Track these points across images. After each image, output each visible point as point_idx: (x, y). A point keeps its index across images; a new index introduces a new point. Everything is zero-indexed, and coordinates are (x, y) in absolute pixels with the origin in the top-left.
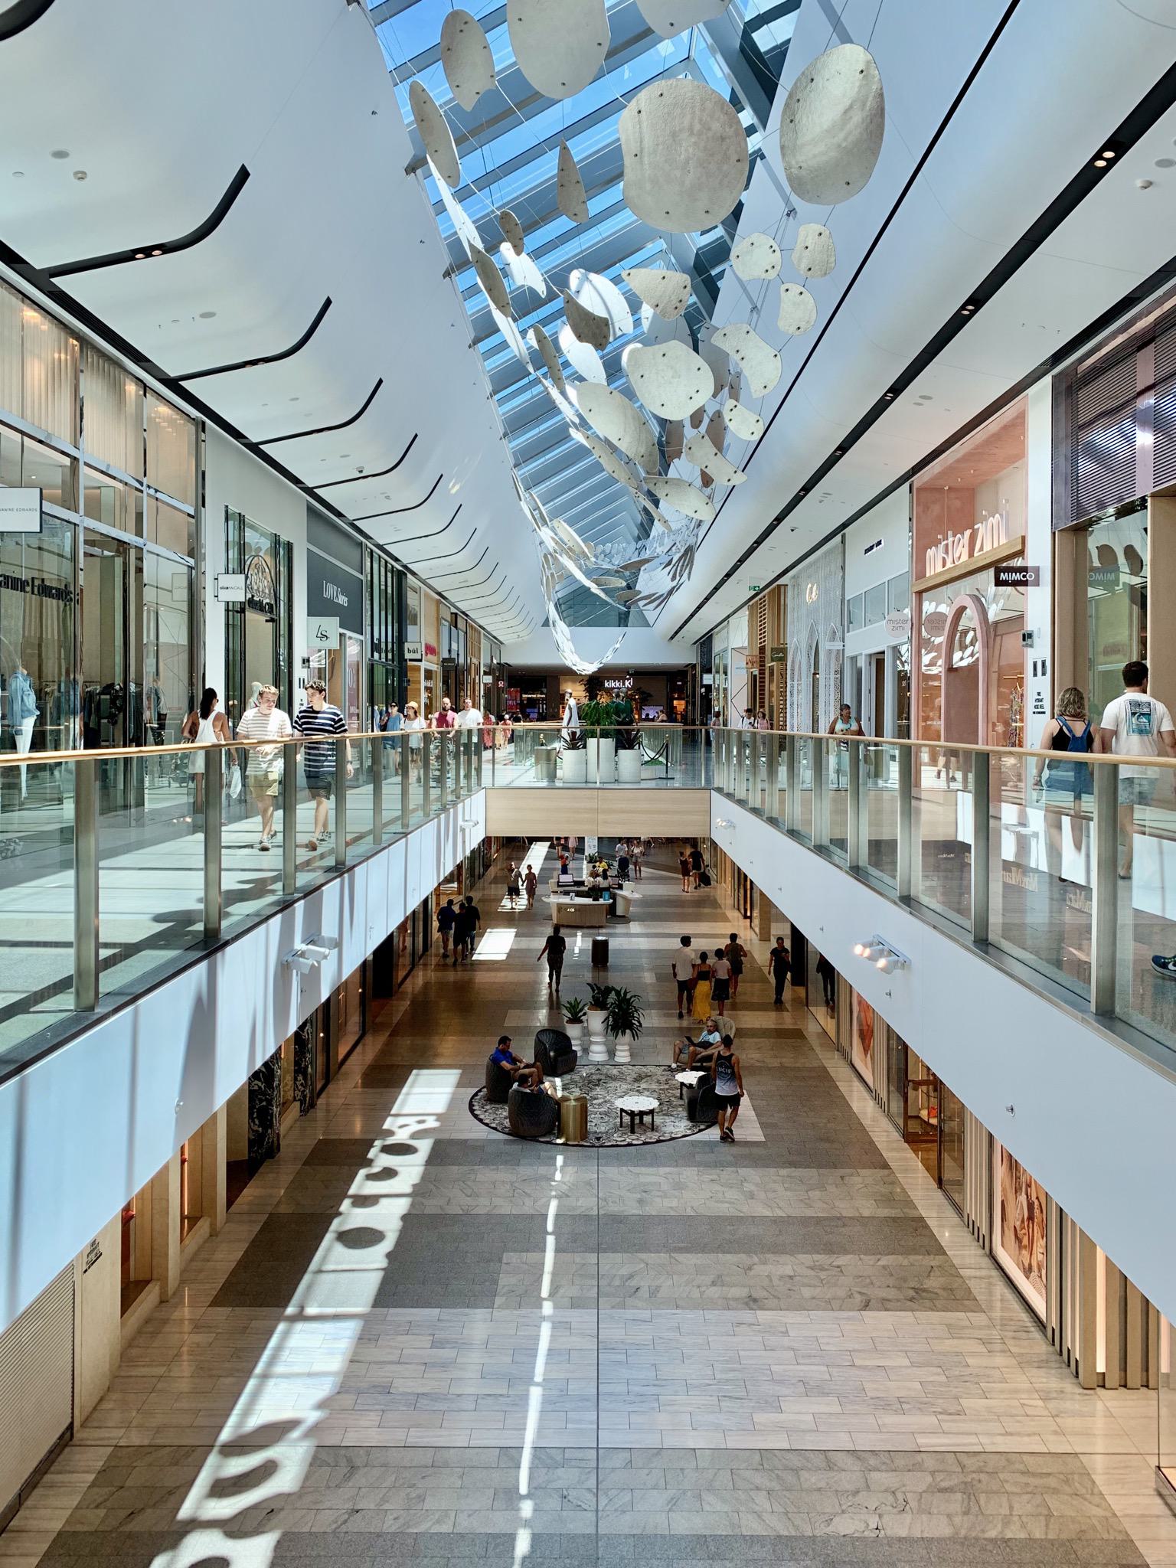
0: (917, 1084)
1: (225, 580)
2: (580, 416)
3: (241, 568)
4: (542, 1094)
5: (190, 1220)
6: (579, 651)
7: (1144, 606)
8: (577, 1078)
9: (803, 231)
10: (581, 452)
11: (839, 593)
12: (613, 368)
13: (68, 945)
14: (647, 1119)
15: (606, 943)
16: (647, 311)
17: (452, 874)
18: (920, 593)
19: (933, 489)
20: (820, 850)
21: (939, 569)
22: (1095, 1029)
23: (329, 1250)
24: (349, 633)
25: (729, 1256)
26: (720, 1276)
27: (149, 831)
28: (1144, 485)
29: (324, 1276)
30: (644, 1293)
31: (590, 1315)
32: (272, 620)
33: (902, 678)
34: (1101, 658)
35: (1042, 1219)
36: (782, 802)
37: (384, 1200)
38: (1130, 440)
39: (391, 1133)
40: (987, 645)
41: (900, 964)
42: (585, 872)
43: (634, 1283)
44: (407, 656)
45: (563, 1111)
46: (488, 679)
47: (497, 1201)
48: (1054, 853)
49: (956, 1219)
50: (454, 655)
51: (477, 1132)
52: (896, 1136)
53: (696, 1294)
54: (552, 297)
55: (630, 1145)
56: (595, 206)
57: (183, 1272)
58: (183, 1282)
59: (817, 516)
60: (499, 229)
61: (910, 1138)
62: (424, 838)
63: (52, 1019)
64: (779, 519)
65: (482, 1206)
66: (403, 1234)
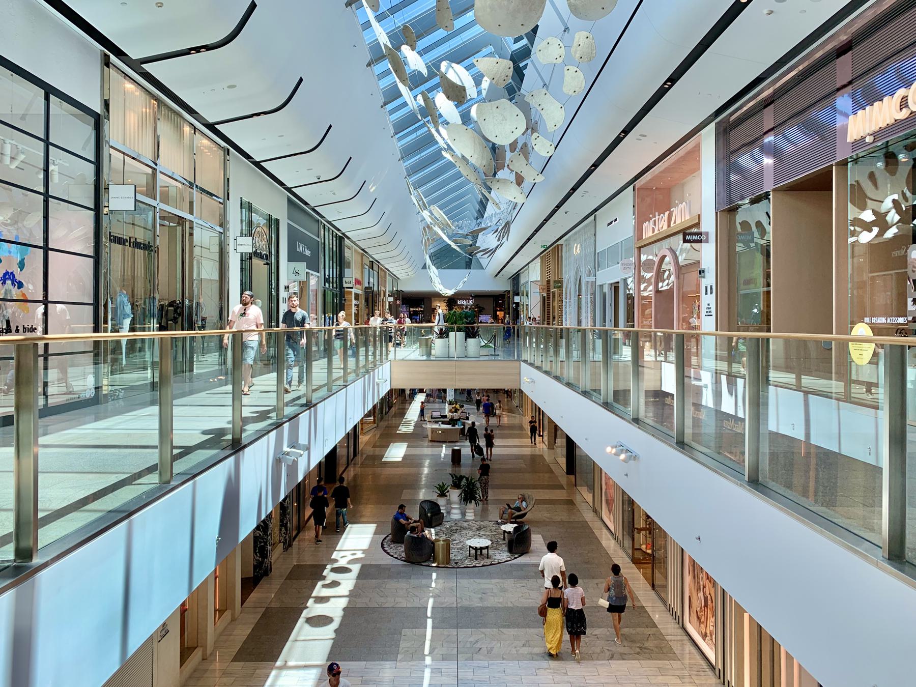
0: (640, 530)
1: (241, 240)
2: (448, 145)
3: (250, 234)
4: (424, 539)
5: (220, 612)
6: (442, 283)
7: (768, 256)
8: (443, 529)
9: (577, 36)
10: (450, 165)
11: (593, 250)
12: (466, 118)
13: (155, 447)
14: (485, 552)
15: (459, 451)
16: (485, 84)
17: (370, 412)
18: (639, 248)
19: (646, 188)
20: (585, 393)
21: (651, 234)
22: (749, 491)
23: (301, 628)
24: (311, 272)
25: (532, 630)
26: (527, 641)
27: (196, 384)
28: (768, 185)
29: (298, 643)
30: (484, 650)
31: (453, 665)
32: (267, 264)
33: (630, 298)
34: (742, 286)
35: (717, 604)
36: (562, 368)
37: (332, 599)
38: (758, 162)
39: (336, 561)
40: (678, 277)
41: (633, 457)
42: (447, 410)
43: (478, 646)
44: (345, 285)
45: (436, 547)
46: (391, 299)
47: (398, 600)
48: (718, 395)
49: (663, 608)
50: (371, 285)
51: (387, 560)
52: (628, 560)
53: (514, 651)
54: (431, 75)
55: (475, 567)
56: (459, 23)
57: (216, 642)
58: (216, 648)
59: (580, 204)
60: (406, 35)
61: (635, 561)
62: (356, 388)
63: (145, 488)
64: (558, 207)
65: (389, 603)
66: (344, 617)
